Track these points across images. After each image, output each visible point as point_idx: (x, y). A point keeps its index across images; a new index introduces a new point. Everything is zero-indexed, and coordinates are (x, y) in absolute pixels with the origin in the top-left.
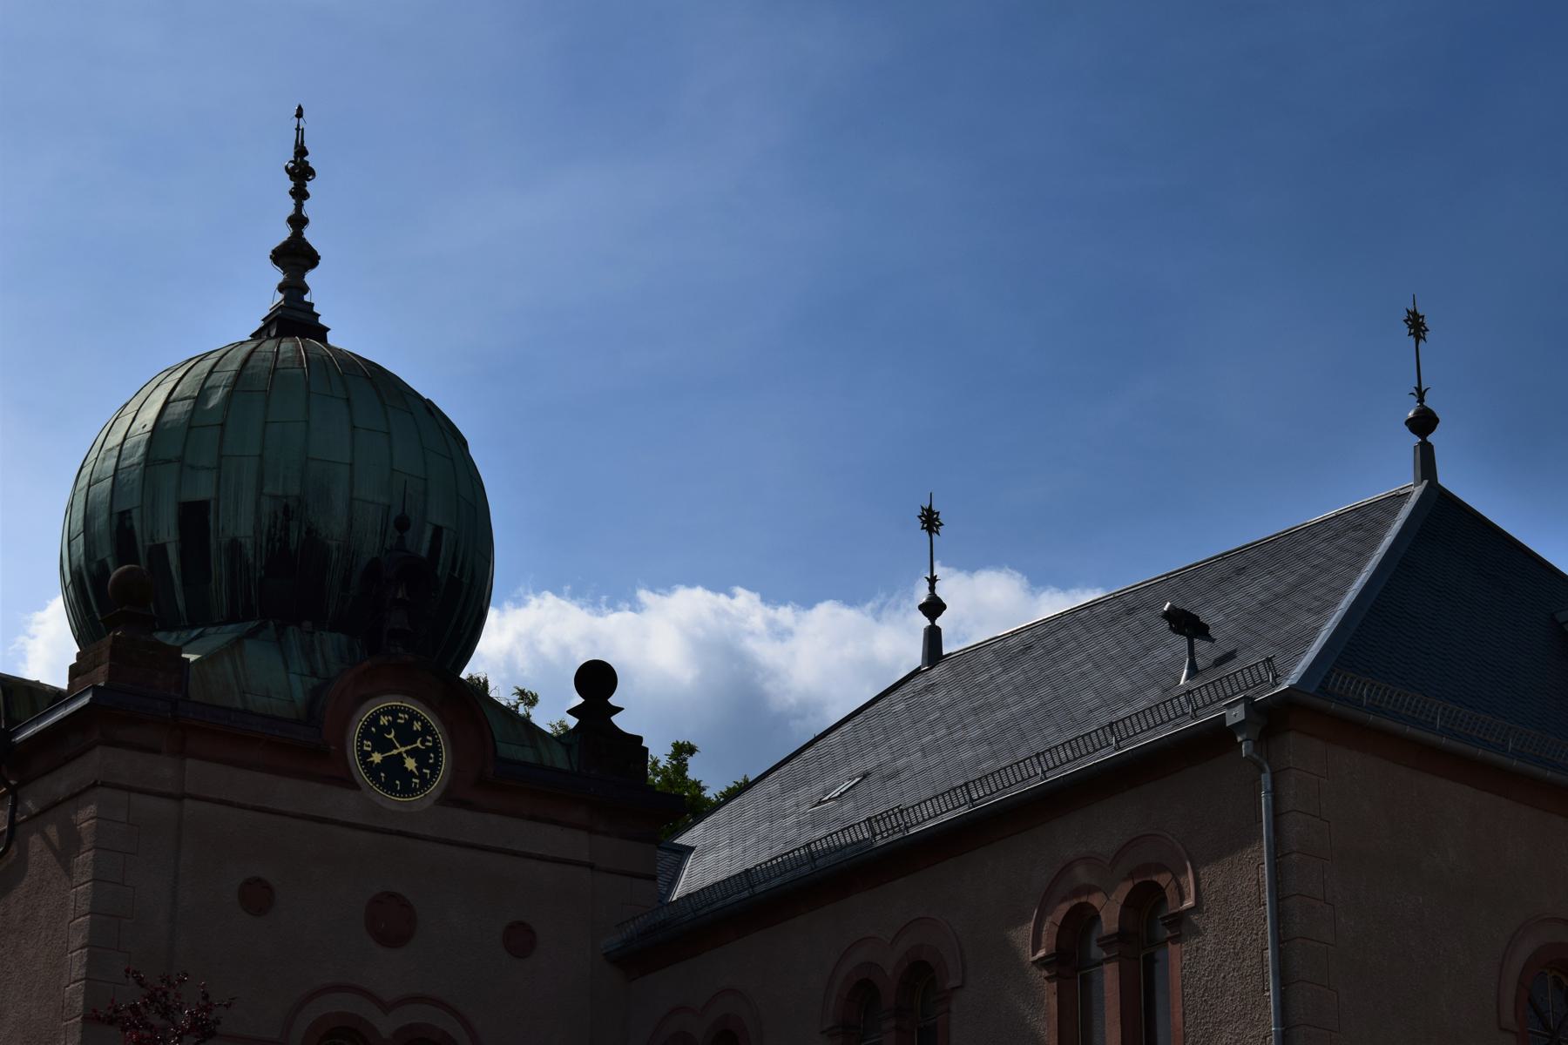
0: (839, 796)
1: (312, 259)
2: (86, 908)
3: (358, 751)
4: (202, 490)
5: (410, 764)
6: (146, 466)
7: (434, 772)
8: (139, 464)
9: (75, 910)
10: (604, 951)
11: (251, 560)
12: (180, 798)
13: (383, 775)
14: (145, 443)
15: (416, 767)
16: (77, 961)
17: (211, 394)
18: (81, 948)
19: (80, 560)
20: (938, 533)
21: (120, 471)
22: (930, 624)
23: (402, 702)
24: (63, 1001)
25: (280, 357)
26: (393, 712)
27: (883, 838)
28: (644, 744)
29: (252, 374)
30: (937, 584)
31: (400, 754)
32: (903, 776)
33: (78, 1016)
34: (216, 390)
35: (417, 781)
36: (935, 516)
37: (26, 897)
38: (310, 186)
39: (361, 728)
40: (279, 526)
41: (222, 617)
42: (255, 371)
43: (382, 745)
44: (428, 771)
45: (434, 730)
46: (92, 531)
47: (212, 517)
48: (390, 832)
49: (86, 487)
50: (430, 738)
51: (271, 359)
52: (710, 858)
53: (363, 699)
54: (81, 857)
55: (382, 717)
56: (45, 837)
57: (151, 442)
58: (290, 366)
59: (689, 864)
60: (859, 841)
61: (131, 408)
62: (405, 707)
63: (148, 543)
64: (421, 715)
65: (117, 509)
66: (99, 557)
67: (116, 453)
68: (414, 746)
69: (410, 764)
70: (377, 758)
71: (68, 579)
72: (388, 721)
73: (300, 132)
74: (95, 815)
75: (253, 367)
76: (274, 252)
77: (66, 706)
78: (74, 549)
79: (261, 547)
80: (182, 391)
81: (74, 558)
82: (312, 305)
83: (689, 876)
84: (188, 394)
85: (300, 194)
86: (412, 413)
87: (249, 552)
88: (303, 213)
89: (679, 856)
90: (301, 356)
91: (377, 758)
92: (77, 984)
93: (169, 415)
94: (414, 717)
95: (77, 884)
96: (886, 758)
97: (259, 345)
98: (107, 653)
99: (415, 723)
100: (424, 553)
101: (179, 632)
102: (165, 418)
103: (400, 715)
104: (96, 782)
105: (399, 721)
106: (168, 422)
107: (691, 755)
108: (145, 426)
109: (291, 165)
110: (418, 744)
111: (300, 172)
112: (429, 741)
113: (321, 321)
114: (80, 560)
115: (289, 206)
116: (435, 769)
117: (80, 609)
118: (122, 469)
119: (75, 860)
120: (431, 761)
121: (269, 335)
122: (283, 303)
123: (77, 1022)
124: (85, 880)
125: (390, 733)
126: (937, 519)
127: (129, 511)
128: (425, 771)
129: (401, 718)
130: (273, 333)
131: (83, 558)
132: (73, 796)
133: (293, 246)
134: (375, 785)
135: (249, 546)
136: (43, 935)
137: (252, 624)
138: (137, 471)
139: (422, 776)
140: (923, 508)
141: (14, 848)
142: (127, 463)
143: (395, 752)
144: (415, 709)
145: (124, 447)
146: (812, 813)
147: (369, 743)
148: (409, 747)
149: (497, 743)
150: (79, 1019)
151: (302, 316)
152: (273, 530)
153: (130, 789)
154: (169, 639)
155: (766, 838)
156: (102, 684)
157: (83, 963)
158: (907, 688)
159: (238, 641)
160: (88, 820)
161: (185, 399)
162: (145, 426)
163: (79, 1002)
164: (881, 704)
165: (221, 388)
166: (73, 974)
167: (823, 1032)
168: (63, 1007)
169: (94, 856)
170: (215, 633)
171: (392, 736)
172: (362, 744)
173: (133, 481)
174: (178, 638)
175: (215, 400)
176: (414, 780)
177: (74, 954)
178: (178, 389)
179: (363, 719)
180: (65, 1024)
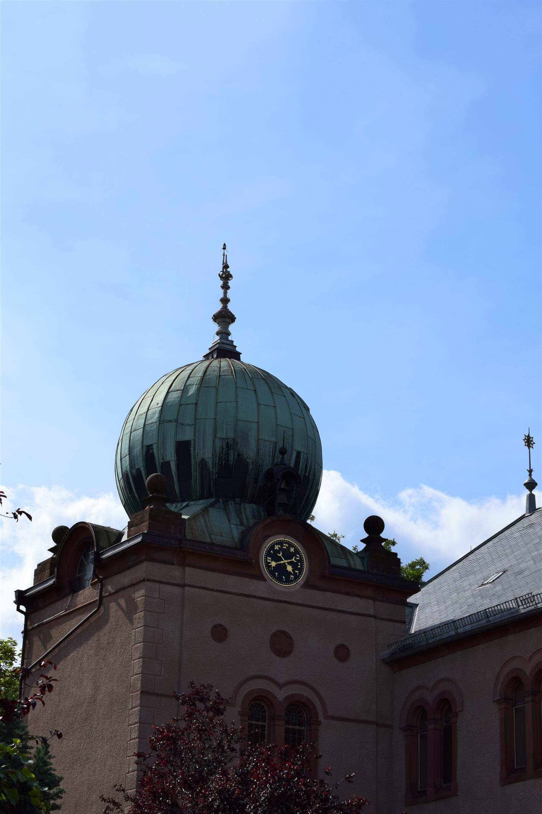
0: (493, 582)
1: (232, 319)
2: (141, 639)
3: (265, 562)
4: (187, 435)
5: (289, 568)
6: (159, 424)
7: (300, 573)
8: (156, 422)
9: (135, 640)
10: (381, 658)
11: (211, 469)
12: (183, 586)
13: (277, 574)
14: (158, 412)
15: (292, 570)
16: (137, 665)
17: (190, 388)
18: (139, 658)
19: (127, 468)
20: (532, 447)
21: (146, 426)
22: (529, 493)
23: (285, 538)
24: (130, 684)
25: (222, 370)
26: (281, 543)
27: (524, 608)
28: (398, 557)
29: (209, 378)
30: (533, 473)
31: (284, 563)
32: (526, 573)
33: (138, 691)
34: (193, 386)
35: (293, 576)
36: (531, 439)
37: (109, 632)
38: (230, 283)
39: (266, 551)
40: (224, 453)
41: (197, 497)
42: (210, 377)
43: (276, 558)
44: (298, 572)
45: (300, 551)
46: (133, 454)
47: (192, 449)
48: (281, 602)
49: (130, 433)
50: (298, 556)
51: (217, 371)
52: (428, 610)
53: (267, 537)
54: (137, 615)
55: (276, 546)
56: (118, 604)
57: (161, 410)
58: (227, 374)
59: (417, 613)
60: (511, 609)
61: (151, 394)
62: (286, 541)
63: (161, 461)
64: (294, 545)
65: (145, 444)
66: (137, 467)
67: (144, 416)
68: (281, 556)
69: (289, 568)
70: (273, 564)
71: (120, 476)
72: (279, 547)
73: (225, 256)
74: (144, 595)
75: (209, 375)
76: (214, 316)
77: (129, 542)
78: (123, 462)
79: (216, 463)
80: (175, 386)
81: (123, 467)
82: (233, 342)
83: (419, 620)
84: (178, 388)
85: (226, 287)
86: (285, 396)
87: (210, 465)
88: (227, 296)
89: (412, 609)
90: (232, 369)
91: (273, 564)
92: (137, 676)
93: (170, 398)
94: (291, 545)
95: (136, 627)
96: (514, 562)
97: (211, 363)
98: (147, 517)
99: (291, 548)
100: (292, 465)
101: (176, 504)
102: (168, 400)
103: (284, 545)
104: (144, 579)
105: (284, 547)
106: (169, 402)
107: (394, 545)
108: (158, 403)
109: (221, 273)
110: (293, 560)
111: (226, 277)
112: (298, 557)
113: (238, 349)
114: (127, 468)
115: (220, 293)
116: (301, 570)
117: (126, 491)
118: (147, 425)
119: (134, 616)
120: (299, 567)
121: (212, 357)
122: (219, 341)
123: (138, 694)
124: (140, 626)
125: (280, 554)
126: (532, 441)
127: (152, 445)
128: (296, 571)
129: (285, 546)
130: (215, 356)
131: (128, 467)
132: (132, 585)
133: (223, 313)
134: (273, 579)
135: (210, 463)
136: (119, 651)
137: (212, 500)
138: (155, 426)
139: (295, 574)
140: (525, 436)
141: (102, 608)
142: (150, 422)
143: (282, 562)
144: (291, 541)
145: (148, 414)
146: (480, 590)
147: (270, 558)
148: (289, 561)
149: (331, 558)
150: (139, 692)
151: (228, 347)
152: (221, 455)
153: (160, 582)
154: (173, 507)
155: (457, 602)
156: (146, 532)
157: (140, 665)
158: (519, 525)
159: (206, 510)
160: (140, 597)
161: (177, 391)
162: (158, 403)
163: (139, 685)
164: (506, 532)
165: (195, 386)
166: (135, 671)
167: (494, 701)
168: (130, 686)
169: (144, 614)
170: (194, 505)
171: (280, 555)
172: (267, 559)
173: (153, 431)
174: (176, 507)
175: (192, 391)
176: (291, 576)
177: (135, 661)
178: (173, 385)
179: (267, 547)
180: (132, 694)
